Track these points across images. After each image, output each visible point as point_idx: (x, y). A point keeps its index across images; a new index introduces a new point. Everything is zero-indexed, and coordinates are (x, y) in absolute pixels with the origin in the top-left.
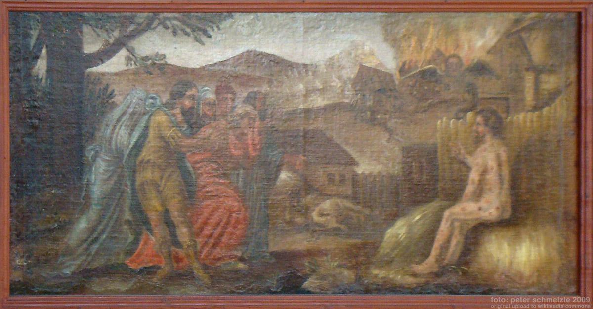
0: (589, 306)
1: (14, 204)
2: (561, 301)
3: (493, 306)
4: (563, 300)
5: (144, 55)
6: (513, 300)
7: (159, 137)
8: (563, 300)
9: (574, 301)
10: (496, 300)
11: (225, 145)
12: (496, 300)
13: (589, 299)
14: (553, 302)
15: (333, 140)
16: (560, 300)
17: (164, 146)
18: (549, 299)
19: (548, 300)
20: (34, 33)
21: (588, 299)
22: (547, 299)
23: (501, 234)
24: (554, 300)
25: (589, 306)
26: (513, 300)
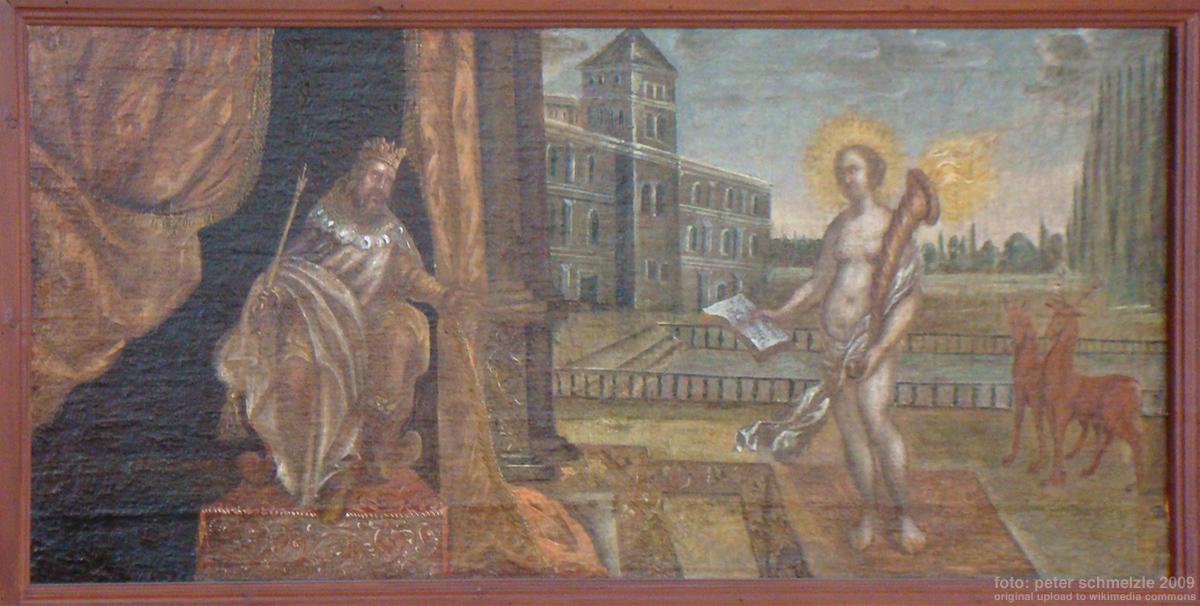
0: (1193, 598)
1: (377, 414)
2: (1136, 587)
3: (998, 597)
4: (1141, 584)
5: (683, 128)
6: (1039, 584)
7: (761, 506)
8: (1141, 584)
9: (1162, 587)
10: (1004, 583)
11: (566, 387)
12: (1004, 583)
13: (1191, 582)
14: (1120, 588)
15: (37, 371)
16: (1134, 583)
17: (355, 278)
18: (1113, 581)
20: (301, 185)
21: (1190, 581)
23: (893, 459)
24: (1122, 584)
25: (1193, 598)
26: (1039, 584)
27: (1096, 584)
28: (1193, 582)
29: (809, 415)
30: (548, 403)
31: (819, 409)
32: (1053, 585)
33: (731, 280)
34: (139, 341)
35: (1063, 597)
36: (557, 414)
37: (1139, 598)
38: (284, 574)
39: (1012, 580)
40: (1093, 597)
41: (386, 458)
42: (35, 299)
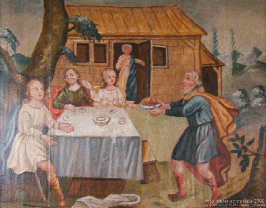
4: (248, 202)
9: (255, 202)
16: (246, 202)
18: (240, 201)
19: (240, 201)
21: (263, 200)
22: (239, 201)
24: (243, 201)
27: (235, 201)
29: (249, 168)
30: (71, 99)
31: (61, 196)
32: (223, 202)
33: (66, 83)
34: (25, 95)
35: (226, 205)
36: (215, 56)
37: (248, 206)
38: (89, 31)
40: (234, 205)
41: (100, 79)
42: (10, 87)
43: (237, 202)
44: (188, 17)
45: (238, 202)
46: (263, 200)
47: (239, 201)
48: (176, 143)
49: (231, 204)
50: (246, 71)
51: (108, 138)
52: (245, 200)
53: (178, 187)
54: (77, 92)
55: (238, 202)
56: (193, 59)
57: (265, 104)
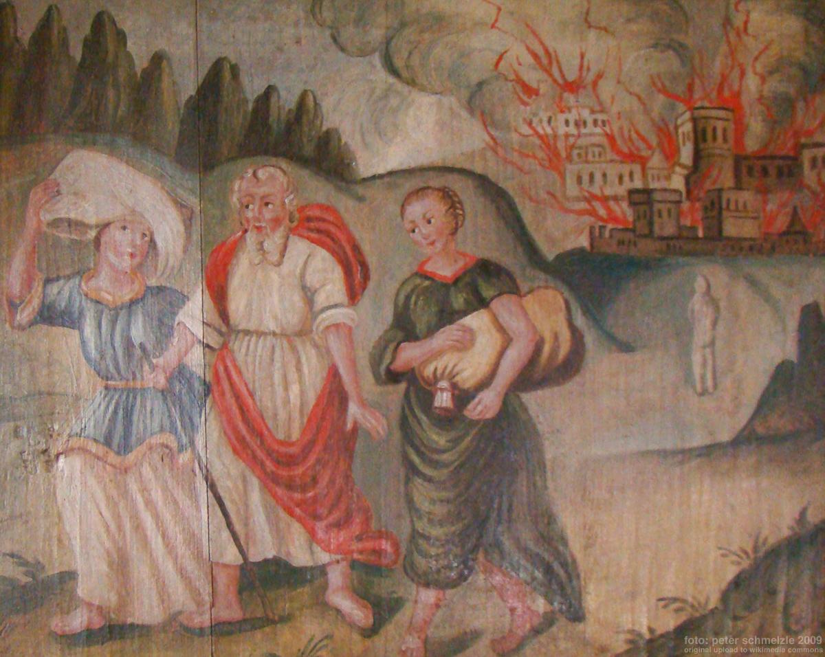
4: (785, 641)
12: (691, 641)
16: (780, 641)
18: (765, 639)
19: (764, 641)
21: (819, 639)
22: (762, 639)
27: (754, 641)
28: (821, 641)
39: (696, 638)
43: (757, 642)
44: (526, 314)
45: (761, 642)
46: (819, 639)
47: (805, 637)
48: (752, 413)
49: (743, 646)
50: (275, 408)
51: (264, 619)
52: (776, 638)
53: (440, 165)
54: (683, 650)
55: (761, 642)
56: (192, 51)
57: (821, 651)
